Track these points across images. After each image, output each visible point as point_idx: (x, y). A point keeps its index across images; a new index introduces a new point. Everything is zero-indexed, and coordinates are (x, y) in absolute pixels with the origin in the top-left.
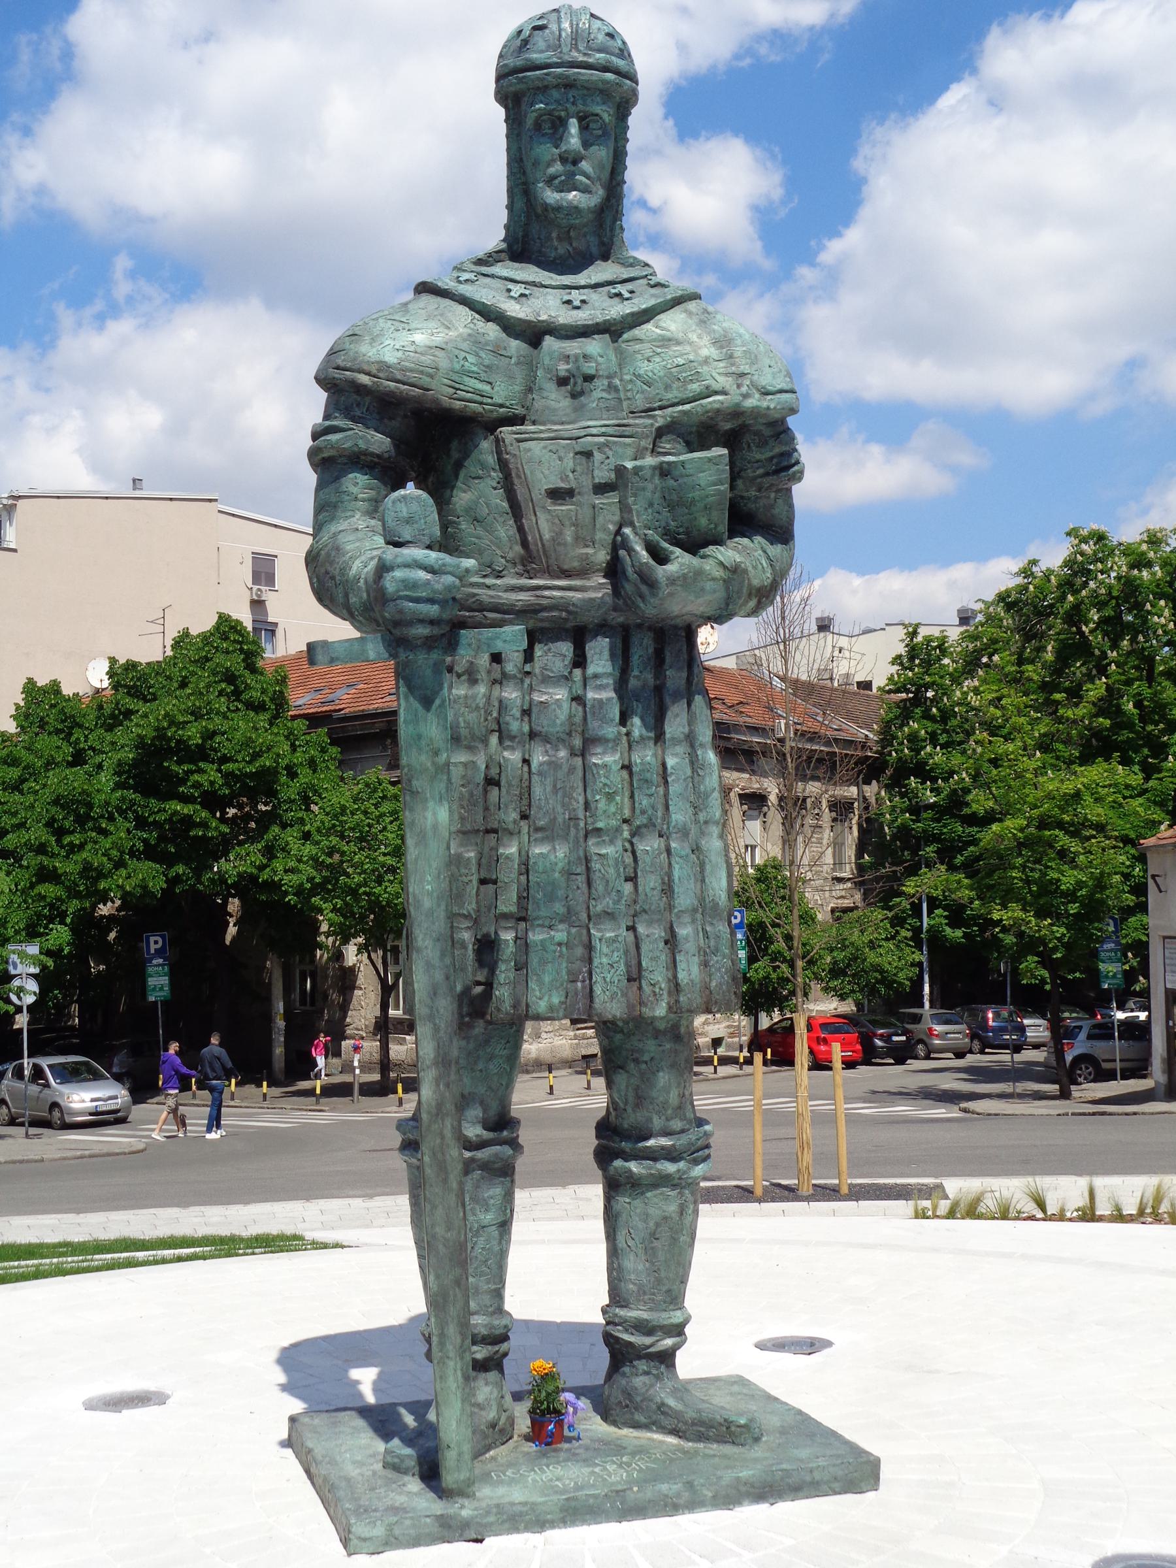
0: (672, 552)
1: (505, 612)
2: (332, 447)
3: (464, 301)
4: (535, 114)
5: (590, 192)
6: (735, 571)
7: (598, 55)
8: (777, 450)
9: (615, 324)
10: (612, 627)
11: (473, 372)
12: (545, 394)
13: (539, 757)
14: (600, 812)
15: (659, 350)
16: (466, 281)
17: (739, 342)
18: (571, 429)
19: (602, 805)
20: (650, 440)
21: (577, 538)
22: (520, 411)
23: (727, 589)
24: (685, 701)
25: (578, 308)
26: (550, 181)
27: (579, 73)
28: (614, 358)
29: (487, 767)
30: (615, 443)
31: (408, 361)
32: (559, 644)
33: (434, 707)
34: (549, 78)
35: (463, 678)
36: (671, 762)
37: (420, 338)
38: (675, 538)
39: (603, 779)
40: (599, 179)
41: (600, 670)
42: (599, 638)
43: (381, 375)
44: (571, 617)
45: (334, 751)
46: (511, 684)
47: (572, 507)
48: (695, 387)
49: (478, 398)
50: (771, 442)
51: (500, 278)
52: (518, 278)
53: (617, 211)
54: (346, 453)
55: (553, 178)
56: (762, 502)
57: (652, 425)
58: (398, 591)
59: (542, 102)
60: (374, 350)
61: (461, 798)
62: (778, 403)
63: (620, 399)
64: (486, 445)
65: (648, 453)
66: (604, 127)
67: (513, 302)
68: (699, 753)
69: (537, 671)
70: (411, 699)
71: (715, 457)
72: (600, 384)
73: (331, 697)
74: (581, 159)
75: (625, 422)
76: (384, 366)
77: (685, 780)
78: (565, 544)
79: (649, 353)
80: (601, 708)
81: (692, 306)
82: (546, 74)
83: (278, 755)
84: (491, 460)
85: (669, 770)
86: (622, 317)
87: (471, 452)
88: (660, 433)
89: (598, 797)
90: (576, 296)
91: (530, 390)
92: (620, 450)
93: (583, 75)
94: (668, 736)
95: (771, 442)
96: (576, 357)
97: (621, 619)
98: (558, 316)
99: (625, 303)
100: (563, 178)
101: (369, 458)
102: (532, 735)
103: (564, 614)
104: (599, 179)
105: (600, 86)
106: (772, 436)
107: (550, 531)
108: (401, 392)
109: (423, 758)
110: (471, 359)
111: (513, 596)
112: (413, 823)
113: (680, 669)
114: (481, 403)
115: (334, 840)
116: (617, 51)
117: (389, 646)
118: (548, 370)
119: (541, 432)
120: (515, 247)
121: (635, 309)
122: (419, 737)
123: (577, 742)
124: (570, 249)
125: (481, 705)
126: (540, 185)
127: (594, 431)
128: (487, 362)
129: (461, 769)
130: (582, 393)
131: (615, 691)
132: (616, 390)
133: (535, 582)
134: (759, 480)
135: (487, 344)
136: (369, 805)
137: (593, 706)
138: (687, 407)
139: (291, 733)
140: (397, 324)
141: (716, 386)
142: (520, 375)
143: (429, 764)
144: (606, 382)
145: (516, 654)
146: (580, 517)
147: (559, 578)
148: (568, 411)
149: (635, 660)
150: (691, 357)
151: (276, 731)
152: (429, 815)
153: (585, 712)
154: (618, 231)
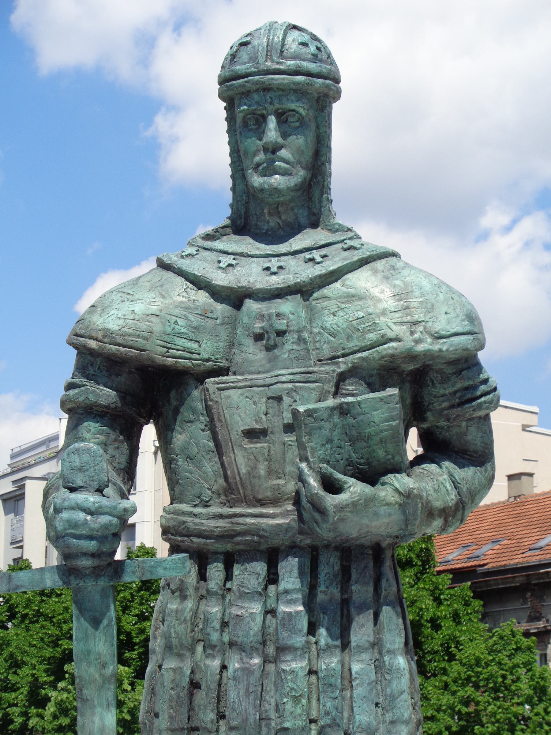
0: (345, 483)
1: (206, 537)
2: (70, 401)
3: (181, 273)
4: (241, 115)
5: (290, 174)
6: (408, 495)
7: (289, 63)
8: (459, 386)
9: (305, 286)
10: (301, 548)
11: (183, 333)
12: (244, 349)
13: (234, 665)
14: (287, 713)
15: (343, 306)
16: (188, 255)
17: (417, 294)
18: (266, 379)
19: (289, 707)
20: (332, 384)
21: (270, 472)
22: (224, 363)
23: (404, 513)
24: (372, 612)
25: (275, 273)
26: (256, 167)
27: (273, 79)
28: (303, 315)
29: (192, 672)
30: (301, 388)
31: (128, 327)
32: (254, 564)
33: (102, 626)
34: (249, 85)
35: (177, 594)
36: (356, 667)
37: (139, 308)
38: (358, 468)
39: (290, 684)
40: (299, 162)
41: (290, 586)
42: (290, 558)
43: (105, 340)
44: (263, 541)
45: (477, 604)
46: (214, 600)
47: (265, 445)
48: (372, 337)
49: (188, 355)
50: (453, 379)
51: (216, 251)
52: (230, 250)
53: (323, 186)
54: (82, 405)
55: (258, 165)
56: (455, 431)
57: (334, 371)
58: (65, 529)
59: (245, 104)
60: (102, 319)
61: (171, 700)
62: (451, 345)
63: (308, 350)
64: (196, 393)
65: (331, 396)
66: (301, 120)
67: (220, 272)
68: (386, 658)
69: (235, 588)
70: (82, 620)
71: (386, 397)
72: (291, 337)
73: (477, 553)
74: (281, 147)
75: (310, 369)
76: (107, 332)
77: (369, 684)
78: (259, 477)
79: (334, 309)
80: (290, 620)
81: (380, 265)
82: (247, 82)
83: (421, 609)
84: (200, 406)
85: (354, 675)
86: (311, 279)
87: (185, 399)
88: (342, 378)
89: (285, 700)
90: (274, 263)
91: (232, 345)
92: (306, 394)
93: (277, 80)
94: (353, 644)
95: (453, 379)
96: (270, 316)
97: (308, 541)
98: (256, 282)
99: (317, 266)
100: (265, 165)
101: (100, 409)
102: (232, 644)
103: (256, 538)
104: (299, 162)
105: (293, 86)
106: (454, 373)
107: (246, 466)
108: (121, 354)
109: (92, 670)
110: (181, 322)
111: (212, 523)
112: (83, 726)
113: (366, 584)
114: (190, 359)
115: (470, 690)
116: (310, 56)
117: (63, 575)
118: (247, 328)
119: (239, 381)
120: (239, 222)
121: (323, 271)
122: (89, 652)
123: (271, 650)
124: (280, 222)
125: (188, 618)
126: (250, 171)
127: (284, 379)
128: (195, 324)
129: (171, 673)
130: (275, 346)
131: (304, 605)
132: (305, 342)
133: (236, 510)
134: (445, 412)
135: (196, 308)
136: (503, 657)
137: (283, 619)
138: (365, 354)
139: (436, 588)
140: (124, 295)
141: (390, 335)
142: (224, 334)
143: (97, 676)
144: (296, 336)
145: (218, 573)
146: (272, 453)
147: (254, 506)
148: (264, 362)
149: (322, 576)
150: (370, 311)
151: (422, 586)
152: (97, 719)
153: (277, 623)
154: (325, 202)
